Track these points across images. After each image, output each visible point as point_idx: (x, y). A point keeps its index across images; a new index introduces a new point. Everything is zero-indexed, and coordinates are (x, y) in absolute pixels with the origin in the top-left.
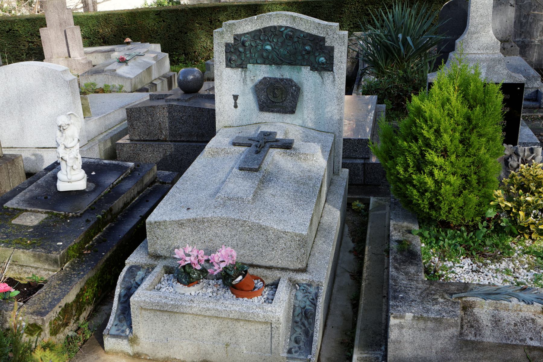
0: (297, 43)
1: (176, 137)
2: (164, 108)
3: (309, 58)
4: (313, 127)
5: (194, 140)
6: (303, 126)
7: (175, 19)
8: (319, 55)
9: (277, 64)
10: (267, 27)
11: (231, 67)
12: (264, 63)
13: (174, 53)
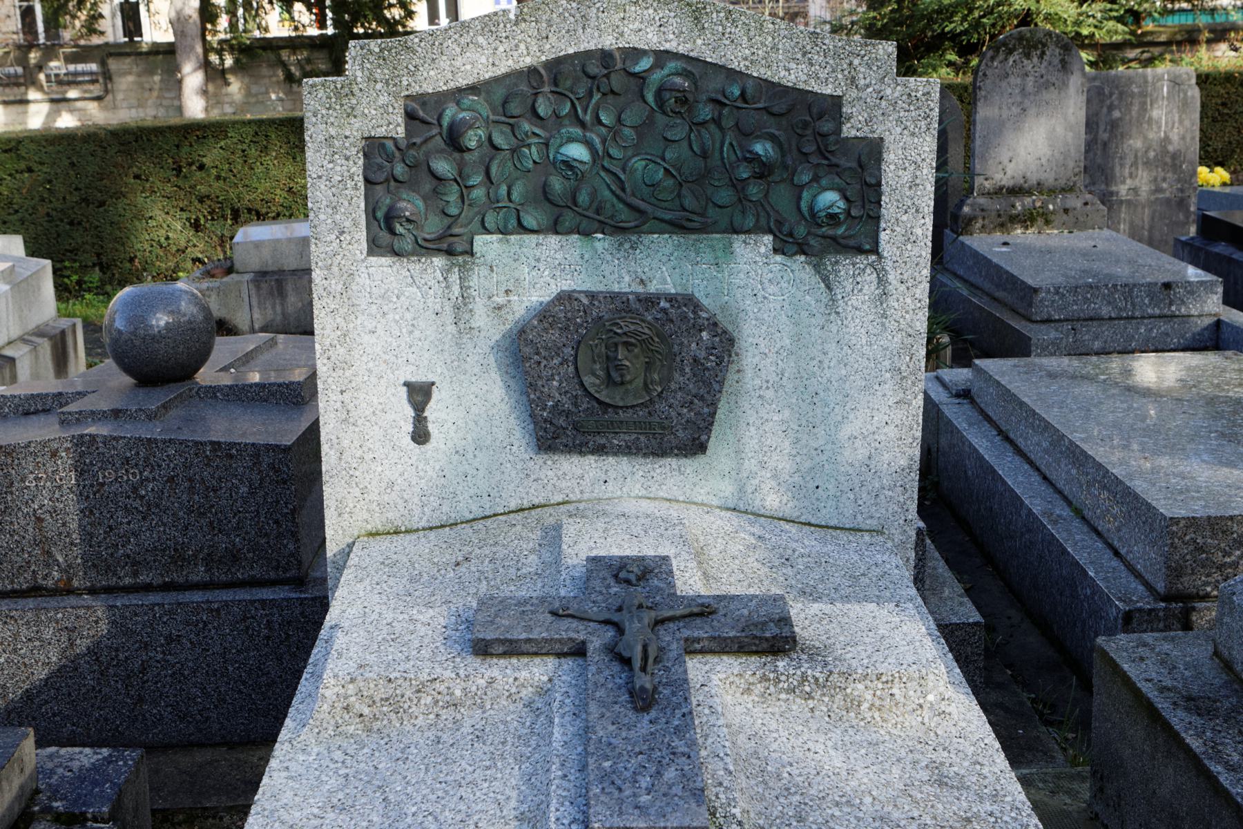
0: (712, 127)
1: (115, 574)
2: (54, 454)
3: (766, 196)
4: (788, 511)
5: (194, 578)
6: (742, 507)
7: (66, 162)
8: (816, 179)
9: (615, 229)
10: (568, 57)
11: (396, 254)
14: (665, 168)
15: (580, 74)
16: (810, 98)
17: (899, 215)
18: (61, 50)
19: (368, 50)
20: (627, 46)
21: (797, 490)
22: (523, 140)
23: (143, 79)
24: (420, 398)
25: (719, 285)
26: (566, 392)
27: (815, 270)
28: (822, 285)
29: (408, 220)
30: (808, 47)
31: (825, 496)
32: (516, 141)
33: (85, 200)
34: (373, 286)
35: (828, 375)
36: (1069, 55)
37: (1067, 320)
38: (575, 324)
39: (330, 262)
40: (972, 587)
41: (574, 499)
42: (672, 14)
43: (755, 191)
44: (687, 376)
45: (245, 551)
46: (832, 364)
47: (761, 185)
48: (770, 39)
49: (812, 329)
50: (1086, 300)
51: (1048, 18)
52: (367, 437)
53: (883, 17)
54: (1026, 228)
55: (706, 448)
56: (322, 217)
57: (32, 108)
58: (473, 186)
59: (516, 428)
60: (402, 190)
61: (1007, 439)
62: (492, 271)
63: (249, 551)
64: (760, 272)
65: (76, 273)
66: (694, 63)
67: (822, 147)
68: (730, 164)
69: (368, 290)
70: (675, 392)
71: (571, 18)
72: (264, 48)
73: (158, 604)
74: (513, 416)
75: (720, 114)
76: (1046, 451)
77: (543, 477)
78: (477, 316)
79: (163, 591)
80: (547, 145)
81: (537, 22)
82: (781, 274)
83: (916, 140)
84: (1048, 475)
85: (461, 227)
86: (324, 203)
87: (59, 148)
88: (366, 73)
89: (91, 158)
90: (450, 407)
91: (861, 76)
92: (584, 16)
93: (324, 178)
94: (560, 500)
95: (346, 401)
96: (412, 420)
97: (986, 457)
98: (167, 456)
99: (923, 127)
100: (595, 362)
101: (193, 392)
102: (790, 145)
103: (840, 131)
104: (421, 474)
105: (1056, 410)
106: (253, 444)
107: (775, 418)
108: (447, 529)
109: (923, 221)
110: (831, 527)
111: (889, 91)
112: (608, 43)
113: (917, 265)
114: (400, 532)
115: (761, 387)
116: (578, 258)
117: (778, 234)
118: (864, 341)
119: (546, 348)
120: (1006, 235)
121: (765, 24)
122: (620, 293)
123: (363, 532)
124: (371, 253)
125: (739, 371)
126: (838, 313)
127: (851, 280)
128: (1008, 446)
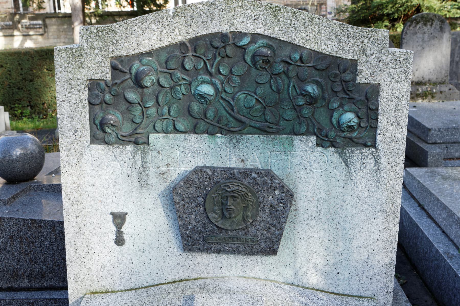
0: (283, 76)
3: (313, 115)
4: (322, 286)
5: (23, 285)
7: (17, 63)
8: (341, 105)
12: (194, 130)
13: (16, 105)
14: (256, 99)
15: (210, 46)
16: (339, 61)
17: (388, 126)
18: (28, 15)
19: (90, 31)
20: (236, 30)
21: (326, 275)
22: (177, 82)
23: (60, 27)
24: (119, 221)
25: (285, 163)
26: (199, 221)
27: (340, 156)
28: (344, 164)
29: (112, 125)
30: (339, 33)
31: (342, 278)
32: (173, 82)
33: (25, 79)
34: (93, 160)
35: (346, 213)
36: (444, 25)
37: (443, 143)
38: (204, 185)
39: (69, 147)
40: (406, 282)
41: (204, 276)
42: (262, 13)
43: (306, 112)
44: (267, 214)
45: (48, 272)
46: (348, 207)
47: (310, 108)
48: (317, 28)
49: (337, 188)
50: (452, 134)
51: (428, 8)
52: (90, 241)
53: (358, 7)
54: (424, 99)
55: (277, 252)
56: (65, 122)
57: (15, 38)
58: (149, 107)
59: (172, 238)
60: (109, 108)
61: (423, 208)
62: (159, 153)
63: (50, 273)
64: (308, 156)
65: (20, 109)
66: (273, 40)
67: (345, 87)
68: (293, 97)
69: (91, 162)
70: (260, 222)
71: (204, 15)
72: (108, 16)
73: (3, 299)
74: (171, 231)
75: (288, 69)
76: (444, 219)
77: (187, 264)
78: (151, 178)
79: (7, 291)
80: (190, 85)
81: (185, 17)
82: (321, 158)
83: (399, 85)
84: (445, 231)
85: (142, 129)
86: (66, 115)
87: (14, 57)
88: (89, 44)
89: (27, 62)
90: (136, 226)
91: (368, 49)
92: (211, 14)
93: (66, 101)
94: (196, 277)
95: (79, 222)
96: (115, 233)
97: (413, 218)
98: (10, 226)
99: (403, 77)
100: (215, 206)
101: (32, 187)
102: (327, 87)
103: (356, 79)
104: (120, 261)
105: (449, 198)
106: (52, 221)
107: (316, 236)
108: (134, 291)
109: (401, 130)
110: (346, 295)
111: (384, 58)
112: (225, 29)
113: (397, 154)
114: (108, 292)
115: (308, 219)
116: (207, 147)
117: (319, 136)
118: (366, 196)
119: (188, 198)
120: (414, 102)
121: (314, 19)
122: (230, 168)
123: (88, 292)
124: (92, 142)
125: (296, 210)
126: (352, 180)
127: (360, 162)
128: (424, 213)
